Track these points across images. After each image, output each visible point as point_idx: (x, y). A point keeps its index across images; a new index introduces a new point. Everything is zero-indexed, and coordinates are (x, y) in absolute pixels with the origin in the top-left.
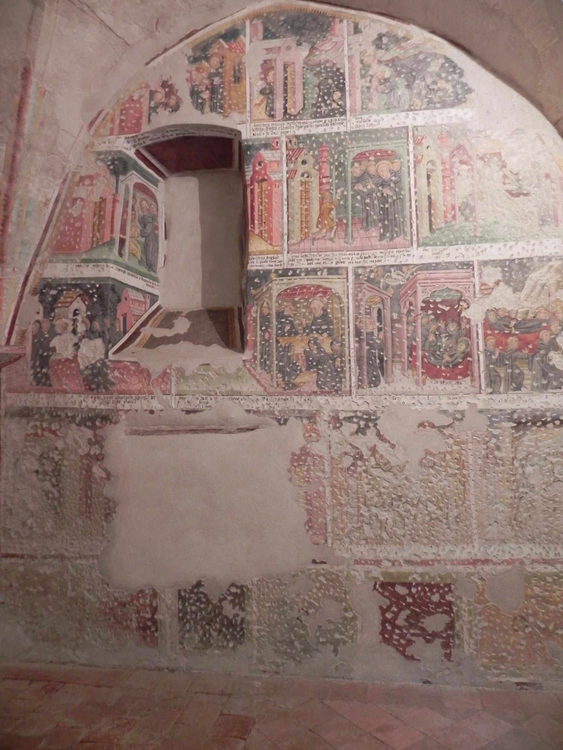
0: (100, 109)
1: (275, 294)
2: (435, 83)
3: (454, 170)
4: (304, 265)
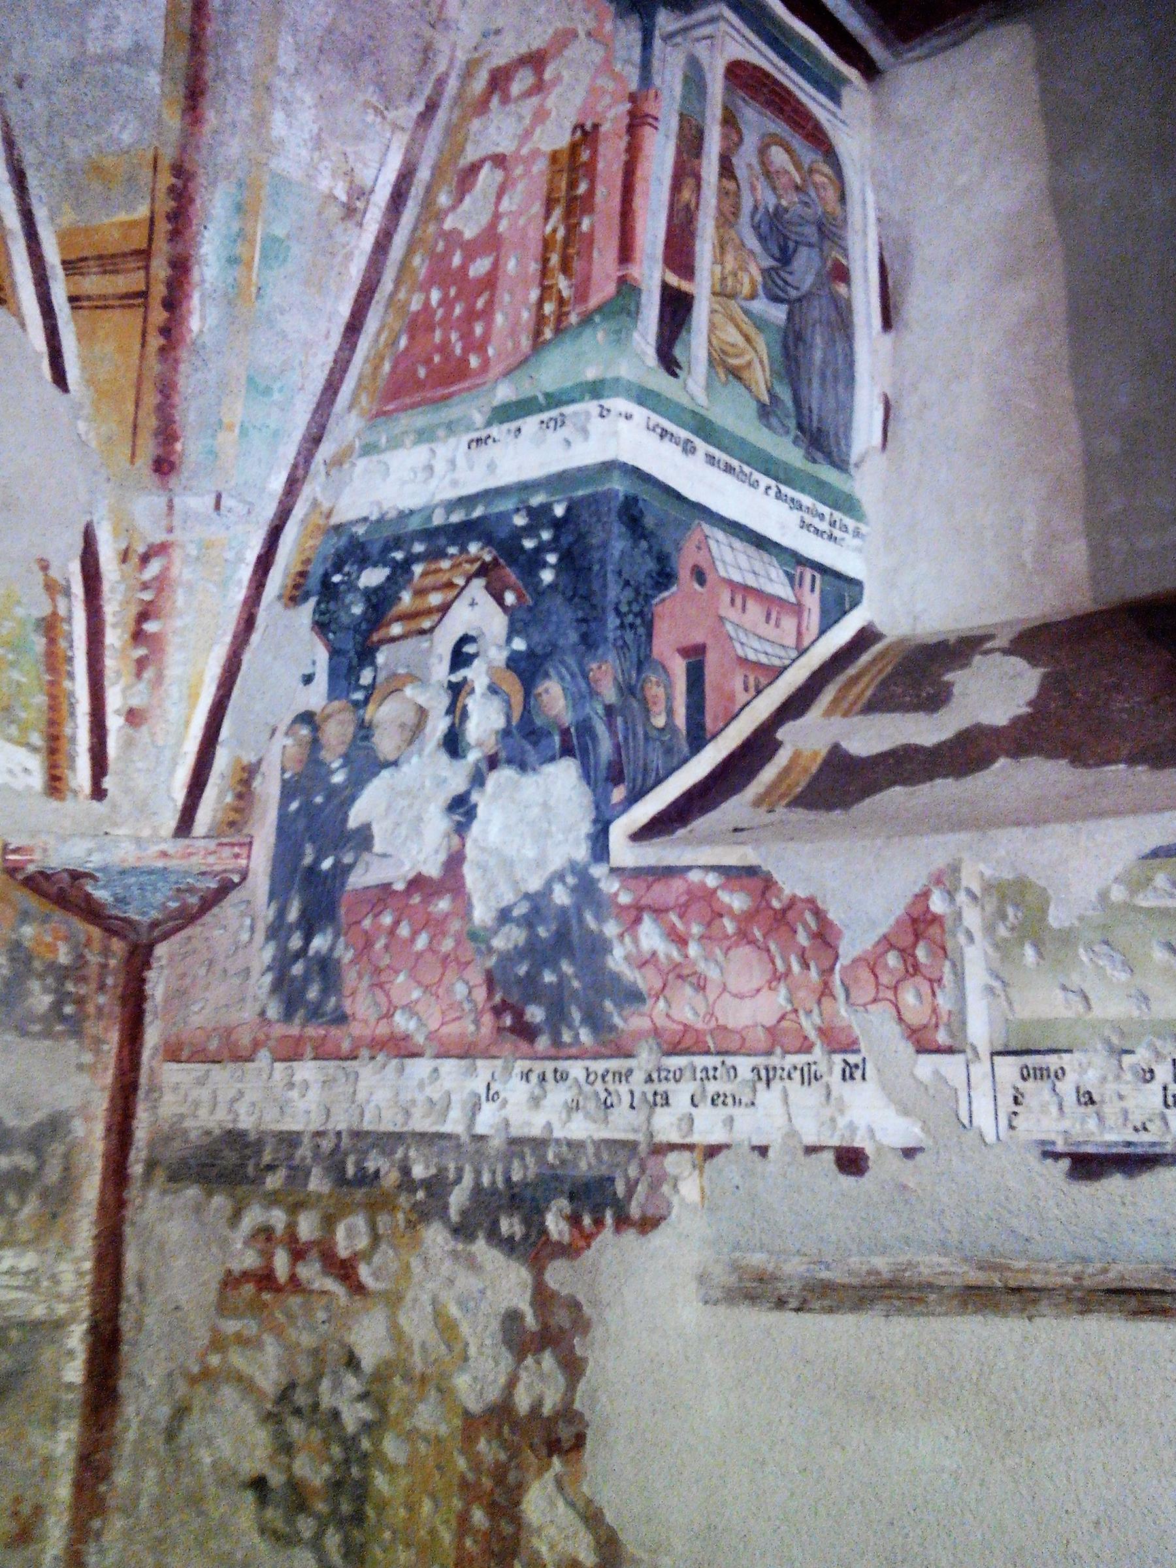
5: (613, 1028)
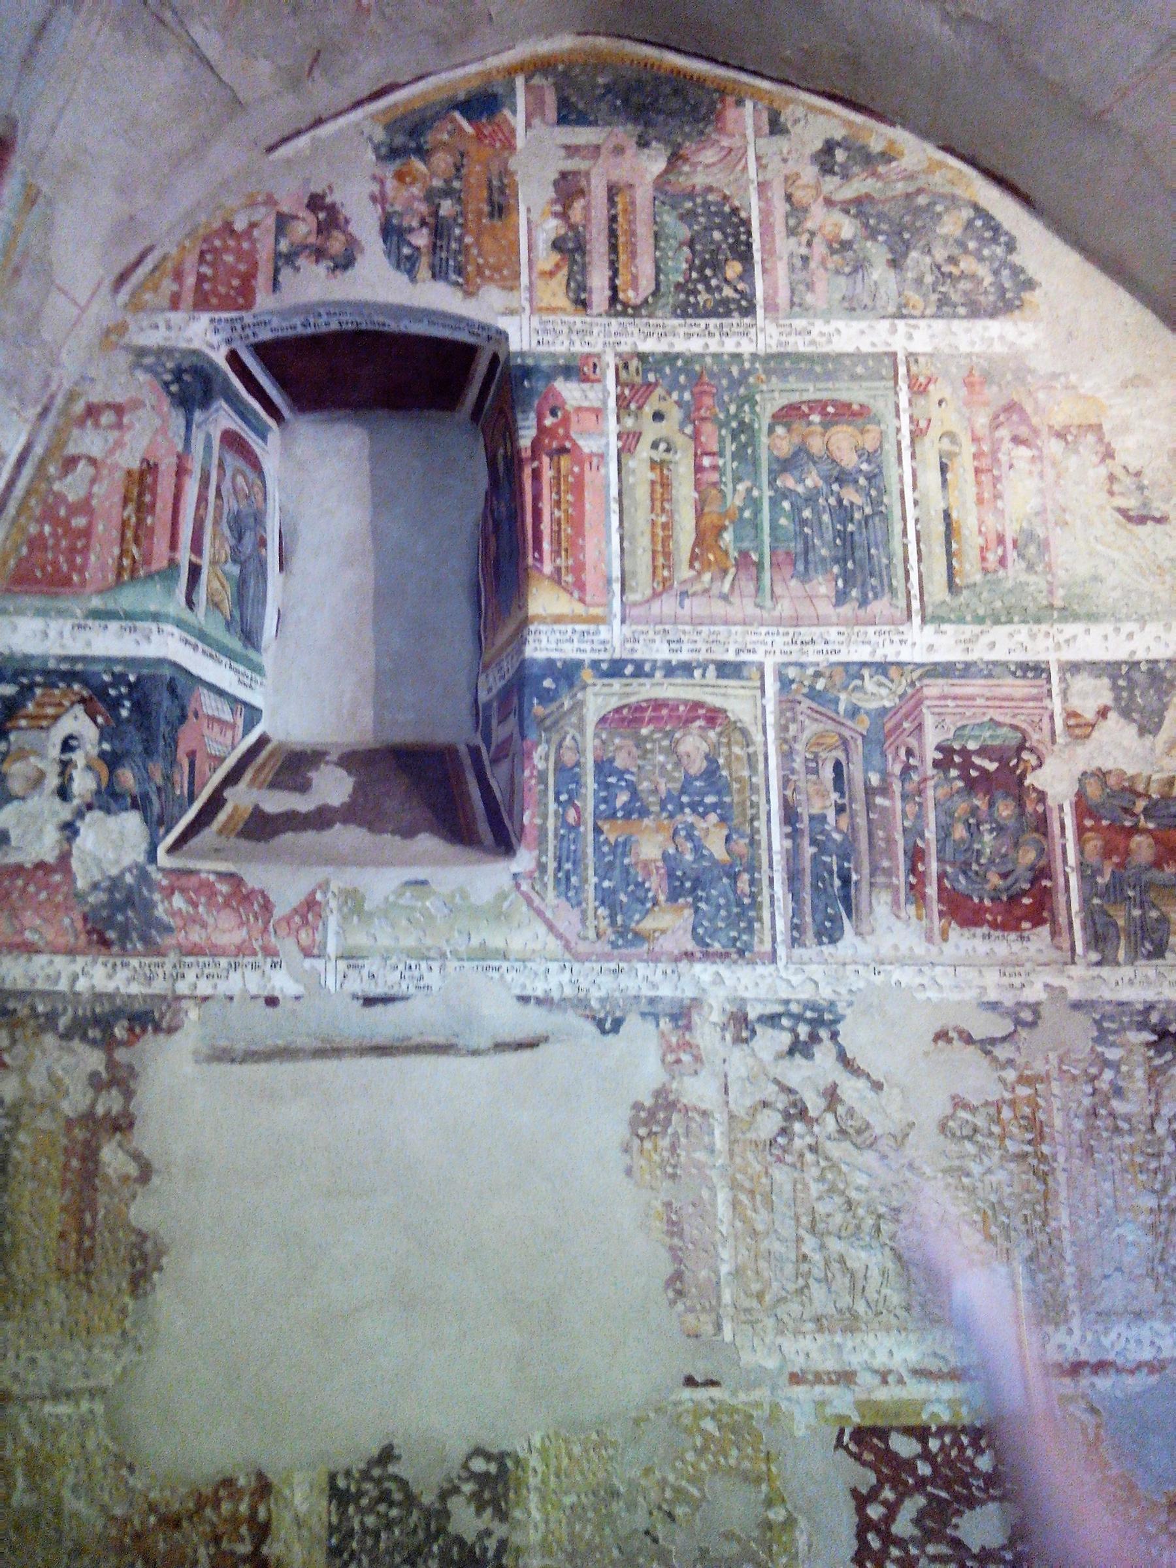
0: (147, 243)
1: (592, 716)
2: (952, 260)
3: (1000, 455)
4: (661, 652)
5: (156, 943)
